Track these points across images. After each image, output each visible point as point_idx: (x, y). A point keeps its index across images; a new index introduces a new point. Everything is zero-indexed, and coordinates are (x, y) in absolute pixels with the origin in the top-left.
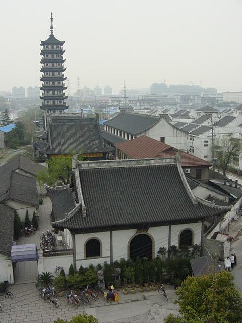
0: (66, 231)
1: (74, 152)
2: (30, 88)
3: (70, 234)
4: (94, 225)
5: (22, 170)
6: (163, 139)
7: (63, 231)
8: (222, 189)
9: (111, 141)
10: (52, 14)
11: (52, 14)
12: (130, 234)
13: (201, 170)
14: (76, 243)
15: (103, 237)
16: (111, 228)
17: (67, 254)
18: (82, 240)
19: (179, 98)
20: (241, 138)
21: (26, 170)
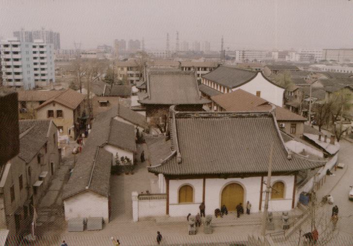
0: (161, 176)
1: (216, 220)
2: (131, 41)
3: (165, 180)
4: (189, 171)
5: (121, 117)
6: (258, 93)
7: (158, 176)
8: (317, 144)
9: (208, 93)
10: (168, 35)
11: (168, 35)
12: (222, 183)
13: (295, 124)
14: (170, 188)
15: (197, 185)
16: (204, 176)
17: (156, 199)
18: (175, 185)
19: (277, 54)
20: (120, 245)
21: (125, 117)
